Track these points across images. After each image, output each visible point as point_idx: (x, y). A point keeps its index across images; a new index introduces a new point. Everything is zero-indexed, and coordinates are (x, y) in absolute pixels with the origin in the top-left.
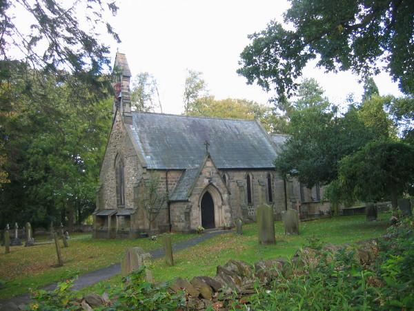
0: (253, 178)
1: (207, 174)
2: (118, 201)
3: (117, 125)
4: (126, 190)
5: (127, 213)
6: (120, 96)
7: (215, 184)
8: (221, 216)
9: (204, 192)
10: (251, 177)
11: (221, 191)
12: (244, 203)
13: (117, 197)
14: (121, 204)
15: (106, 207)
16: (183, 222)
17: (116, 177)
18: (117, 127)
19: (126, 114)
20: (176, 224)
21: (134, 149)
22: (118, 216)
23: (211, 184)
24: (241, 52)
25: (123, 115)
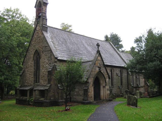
0: (114, 71)
1: (99, 65)
2: (34, 80)
3: (37, 33)
4: (41, 74)
5: (42, 88)
6: (40, 15)
7: (102, 71)
8: (105, 92)
9: (96, 76)
10: (113, 71)
11: (106, 77)
12: (120, 85)
13: (34, 78)
14: (37, 82)
15: (26, 84)
16: (81, 96)
17: (34, 65)
18: (37, 34)
19: (44, 25)
20: (74, 97)
21: (49, 46)
22: (35, 90)
23: (100, 71)
24: (48, 6)
25: (42, 26)
